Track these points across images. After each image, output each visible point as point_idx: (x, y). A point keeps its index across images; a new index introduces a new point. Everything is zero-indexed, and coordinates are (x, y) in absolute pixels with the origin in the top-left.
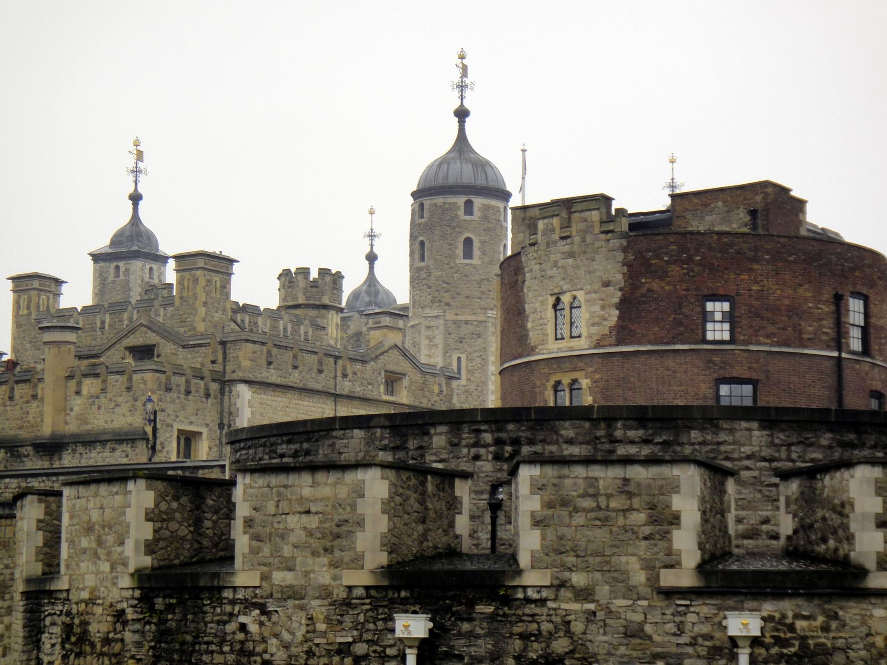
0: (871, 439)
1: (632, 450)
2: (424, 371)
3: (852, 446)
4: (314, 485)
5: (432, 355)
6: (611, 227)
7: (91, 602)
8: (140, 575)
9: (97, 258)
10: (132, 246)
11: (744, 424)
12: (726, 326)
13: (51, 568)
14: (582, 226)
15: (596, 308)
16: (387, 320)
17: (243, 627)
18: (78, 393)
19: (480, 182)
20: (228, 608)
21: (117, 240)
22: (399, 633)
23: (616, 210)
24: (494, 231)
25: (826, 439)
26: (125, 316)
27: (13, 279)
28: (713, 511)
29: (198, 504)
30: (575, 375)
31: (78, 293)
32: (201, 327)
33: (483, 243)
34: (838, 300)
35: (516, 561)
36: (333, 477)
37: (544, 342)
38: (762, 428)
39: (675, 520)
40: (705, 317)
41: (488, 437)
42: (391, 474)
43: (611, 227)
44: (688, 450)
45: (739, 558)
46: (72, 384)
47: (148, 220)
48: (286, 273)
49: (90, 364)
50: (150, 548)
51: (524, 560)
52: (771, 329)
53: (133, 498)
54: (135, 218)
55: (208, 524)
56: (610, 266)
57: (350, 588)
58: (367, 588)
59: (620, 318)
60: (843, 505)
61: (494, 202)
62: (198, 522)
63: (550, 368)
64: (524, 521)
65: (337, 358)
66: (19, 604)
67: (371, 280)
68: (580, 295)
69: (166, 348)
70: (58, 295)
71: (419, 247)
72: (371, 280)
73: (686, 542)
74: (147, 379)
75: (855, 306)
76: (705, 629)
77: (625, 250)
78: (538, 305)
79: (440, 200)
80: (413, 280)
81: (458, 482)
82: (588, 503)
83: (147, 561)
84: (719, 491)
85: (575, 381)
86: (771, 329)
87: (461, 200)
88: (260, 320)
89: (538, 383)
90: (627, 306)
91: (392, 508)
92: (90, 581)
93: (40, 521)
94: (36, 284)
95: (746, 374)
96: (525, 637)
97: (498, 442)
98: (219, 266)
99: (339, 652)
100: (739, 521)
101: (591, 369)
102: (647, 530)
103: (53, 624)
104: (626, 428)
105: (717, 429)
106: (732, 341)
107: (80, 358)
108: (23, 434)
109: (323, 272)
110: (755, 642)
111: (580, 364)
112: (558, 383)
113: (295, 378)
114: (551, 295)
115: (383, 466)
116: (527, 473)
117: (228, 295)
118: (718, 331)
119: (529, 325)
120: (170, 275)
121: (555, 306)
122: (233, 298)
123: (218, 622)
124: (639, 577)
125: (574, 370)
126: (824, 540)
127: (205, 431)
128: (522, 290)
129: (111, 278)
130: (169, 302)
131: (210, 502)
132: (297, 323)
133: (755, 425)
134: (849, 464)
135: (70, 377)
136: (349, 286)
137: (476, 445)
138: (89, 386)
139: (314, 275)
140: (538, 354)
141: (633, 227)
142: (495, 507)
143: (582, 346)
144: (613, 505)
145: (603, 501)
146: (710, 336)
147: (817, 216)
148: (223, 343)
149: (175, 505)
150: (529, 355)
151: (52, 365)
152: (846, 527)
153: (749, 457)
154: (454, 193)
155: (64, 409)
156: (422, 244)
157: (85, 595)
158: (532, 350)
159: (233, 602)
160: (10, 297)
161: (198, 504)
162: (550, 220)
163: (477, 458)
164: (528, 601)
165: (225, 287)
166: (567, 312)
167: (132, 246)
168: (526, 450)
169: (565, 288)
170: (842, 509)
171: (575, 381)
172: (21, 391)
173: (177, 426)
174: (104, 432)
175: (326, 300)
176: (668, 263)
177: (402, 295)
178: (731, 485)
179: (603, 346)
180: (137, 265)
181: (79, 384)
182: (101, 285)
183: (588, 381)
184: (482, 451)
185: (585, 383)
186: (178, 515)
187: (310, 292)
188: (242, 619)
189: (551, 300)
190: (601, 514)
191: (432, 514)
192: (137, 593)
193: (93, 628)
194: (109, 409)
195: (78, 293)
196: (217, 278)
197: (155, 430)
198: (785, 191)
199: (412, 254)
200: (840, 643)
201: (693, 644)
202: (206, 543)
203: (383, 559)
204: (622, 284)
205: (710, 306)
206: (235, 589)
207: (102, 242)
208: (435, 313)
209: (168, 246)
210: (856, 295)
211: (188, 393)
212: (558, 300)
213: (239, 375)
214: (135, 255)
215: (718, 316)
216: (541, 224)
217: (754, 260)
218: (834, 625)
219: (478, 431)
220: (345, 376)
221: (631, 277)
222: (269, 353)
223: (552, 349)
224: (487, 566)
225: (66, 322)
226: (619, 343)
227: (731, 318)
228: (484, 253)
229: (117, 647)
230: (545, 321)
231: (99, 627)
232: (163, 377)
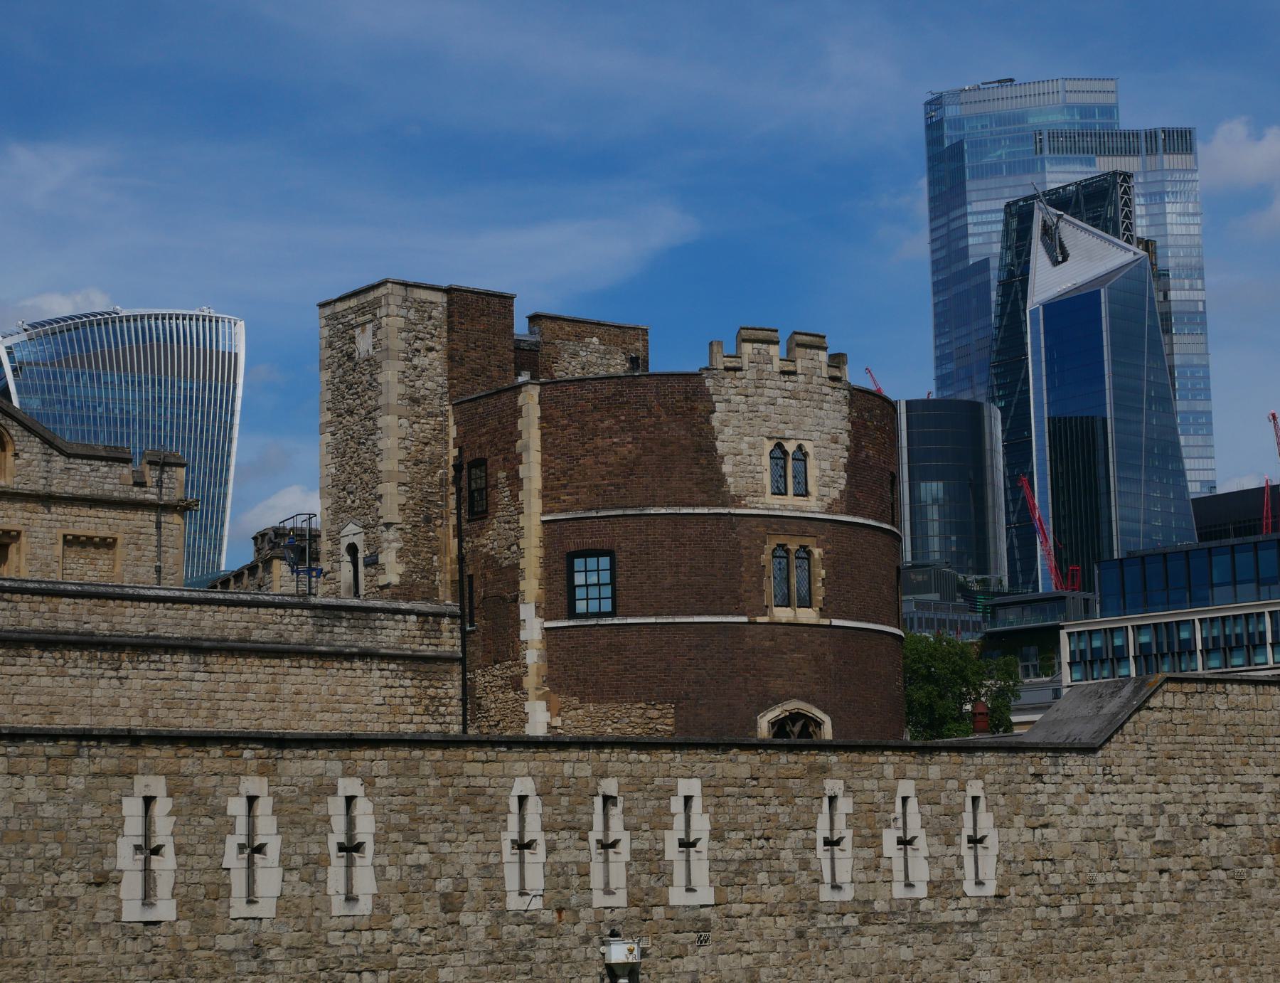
15: (826, 465)
23: (534, 319)
30: (806, 541)
59: (848, 482)
63: (768, 527)
78: (744, 446)
89: (744, 543)
101: (823, 537)
111: (810, 530)
114: (769, 438)
119: (726, 468)
125: (803, 535)
128: (708, 421)
140: (745, 506)
143: (812, 506)
150: (724, 505)
162: (765, 346)
169: (788, 433)
179: (835, 513)
183: (820, 550)
189: (769, 446)
204: (848, 443)
221: (855, 438)
226: (847, 514)
230: (759, 469)
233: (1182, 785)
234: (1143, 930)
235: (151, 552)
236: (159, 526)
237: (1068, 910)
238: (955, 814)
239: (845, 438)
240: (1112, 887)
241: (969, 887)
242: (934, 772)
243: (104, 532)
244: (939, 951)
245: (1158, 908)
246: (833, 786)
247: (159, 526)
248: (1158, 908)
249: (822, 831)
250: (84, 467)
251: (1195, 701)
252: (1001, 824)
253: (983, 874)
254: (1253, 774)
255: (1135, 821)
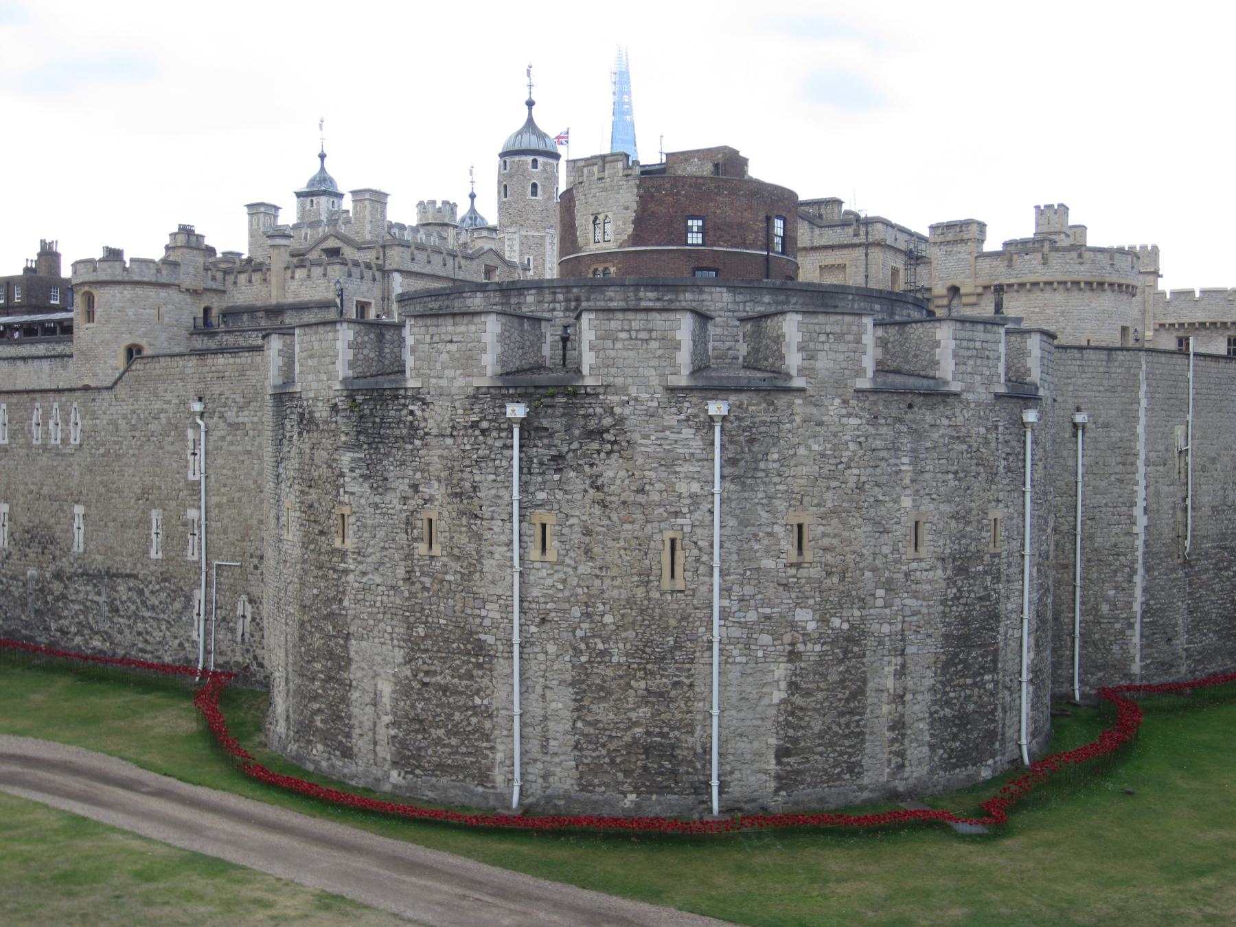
0: (793, 300)
1: (650, 304)
2: (511, 265)
3: (783, 303)
4: (455, 325)
5: (513, 256)
6: (630, 172)
7: (316, 399)
8: (345, 381)
9: (299, 195)
10: (320, 189)
11: (718, 289)
12: (700, 235)
13: (289, 380)
14: (612, 171)
15: (619, 223)
16: (485, 233)
17: (412, 413)
18: (292, 278)
19: (542, 147)
20: (402, 401)
21: (312, 183)
22: (508, 415)
24: (552, 178)
25: (767, 299)
26: (320, 230)
27: (248, 206)
28: (700, 340)
29: (381, 338)
30: (607, 265)
31: (288, 216)
32: (368, 237)
33: (543, 186)
34: (768, 219)
35: (580, 371)
36: (466, 319)
37: (587, 244)
38: (728, 292)
39: (677, 346)
40: (688, 230)
41: (560, 297)
42: (503, 319)
43: (630, 172)
44: (684, 304)
45: (714, 369)
46: (289, 272)
47: (331, 171)
48: (421, 203)
49: (300, 259)
50: (352, 365)
51: (585, 370)
52: (727, 237)
53: (340, 335)
54: (323, 169)
55: (387, 350)
56: (628, 197)
57: (478, 388)
58: (489, 388)
60: (778, 337)
61: (550, 161)
62: (381, 350)
64: (585, 346)
65: (455, 256)
66: (269, 402)
67: (473, 210)
68: (610, 215)
69: (349, 252)
70: (276, 217)
71: (504, 189)
72: (473, 210)
73: (684, 357)
74: (336, 271)
75: (779, 224)
76: (695, 411)
77: (638, 187)
79: (516, 159)
80: (500, 209)
81: (543, 324)
82: (624, 335)
83: (350, 373)
84: (704, 329)
85: (606, 269)
86: (727, 237)
87: (530, 159)
88: (406, 233)
90: (638, 222)
91: (502, 338)
92: (315, 385)
93: (280, 350)
94: (262, 209)
95: (712, 265)
96: (586, 416)
97: (567, 300)
98: (378, 199)
99: (471, 427)
100: (714, 349)
102: (660, 352)
103: (292, 413)
104: (646, 291)
105: (701, 292)
106: (703, 244)
107: (293, 256)
108: (259, 304)
109: (445, 203)
110: (724, 418)
112: (596, 270)
113: (427, 270)
115: (497, 313)
116: (585, 317)
117: (385, 217)
118: (695, 239)
120: (347, 204)
121: (594, 222)
122: (388, 218)
123: (396, 410)
124: (655, 381)
125: (606, 262)
126: (766, 359)
127: (373, 301)
129: (308, 207)
130: (347, 222)
131: (388, 337)
132: (429, 235)
133: (724, 290)
134: (783, 313)
135: (287, 268)
136: (462, 211)
137: (554, 301)
138: (300, 273)
139: (439, 204)
141: (642, 173)
142: (565, 340)
143: (612, 247)
144: (640, 336)
145: (634, 334)
146: (690, 241)
147: (756, 171)
148: (384, 247)
149: (366, 338)
151: (278, 261)
152: (779, 350)
153: (721, 309)
154: (527, 154)
155: (283, 287)
156: (505, 187)
157: (311, 395)
158: (579, 250)
159: (405, 397)
160: (246, 218)
161: (381, 338)
163: (554, 310)
164: (588, 395)
165: (383, 213)
166: (601, 226)
167: (320, 189)
168: (584, 304)
170: (778, 339)
171: (606, 269)
172: (256, 277)
173: (355, 299)
174: (310, 302)
175: (447, 221)
176: (666, 195)
177: (492, 218)
178: (710, 327)
180: (323, 199)
181: (293, 272)
182: (303, 212)
184: (558, 305)
185: (612, 270)
186: (368, 346)
187: (437, 219)
188: (411, 407)
189: (592, 218)
190: (633, 342)
191: (528, 343)
192: (345, 393)
193: (317, 415)
194: (312, 287)
195: (288, 216)
196: (378, 206)
197: (342, 301)
198: (736, 152)
199: (499, 193)
200: (775, 419)
201: (688, 420)
202: (387, 362)
203: (499, 370)
205: (690, 223)
206: (406, 389)
207: (302, 186)
208: (513, 230)
209: (343, 186)
210: (779, 217)
211: (362, 278)
212: (596, 218)
213: (395, 266)
214: (324, 193)
215: (695, 229)
216: (585, 170)
217: (718, 194)
218: (771, 408)
219: (555, 293)
220: (460, 267)
222: (412, 254)
223: (593, 249)
224: (561, 374)
225: (282, 234)
226: (633, 246)
227: (702, 230)
228: (544, 192)
229: (333, 426)
231: (322, 412)
232: (346, 268)
233: (142, 402)
234: (125, 460)
235: (863, 268)
236: (867, 255)
237: (102, 451)
238: (69, 414)
239: (635, 206)
240: (116, 443)
241: (72, 441)
242: (63, 399)
243: (839, 261)
244: (63, 463)
245: (131, 452)
246: (37, 405)
247: (867, 255)
248: (131, 452)
249: (34, 421)
250: (829, 231)
251: (148, 366)
252: (82, 418)
253: (75, 438)
254: (168, 396)
255: (125, 417)
